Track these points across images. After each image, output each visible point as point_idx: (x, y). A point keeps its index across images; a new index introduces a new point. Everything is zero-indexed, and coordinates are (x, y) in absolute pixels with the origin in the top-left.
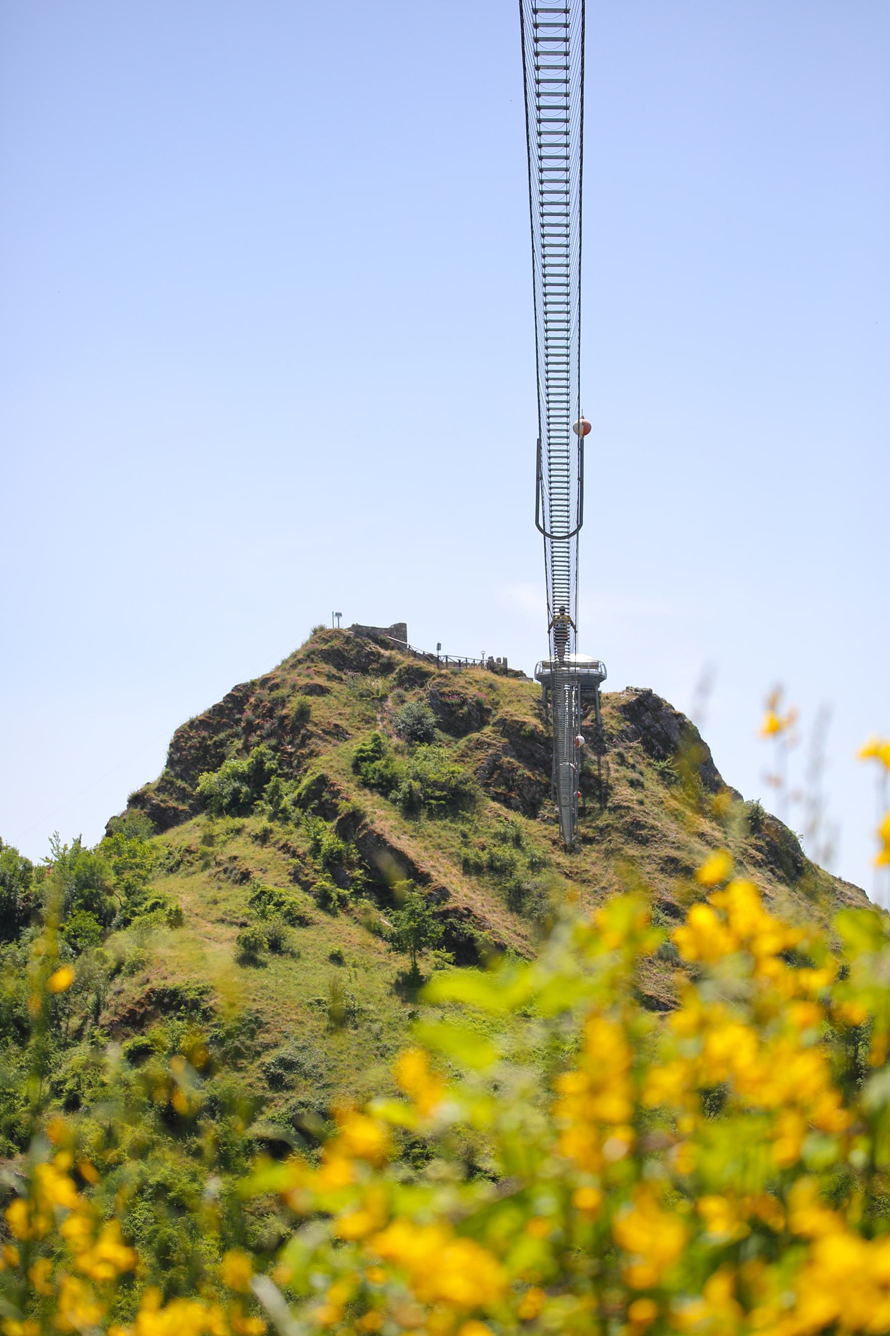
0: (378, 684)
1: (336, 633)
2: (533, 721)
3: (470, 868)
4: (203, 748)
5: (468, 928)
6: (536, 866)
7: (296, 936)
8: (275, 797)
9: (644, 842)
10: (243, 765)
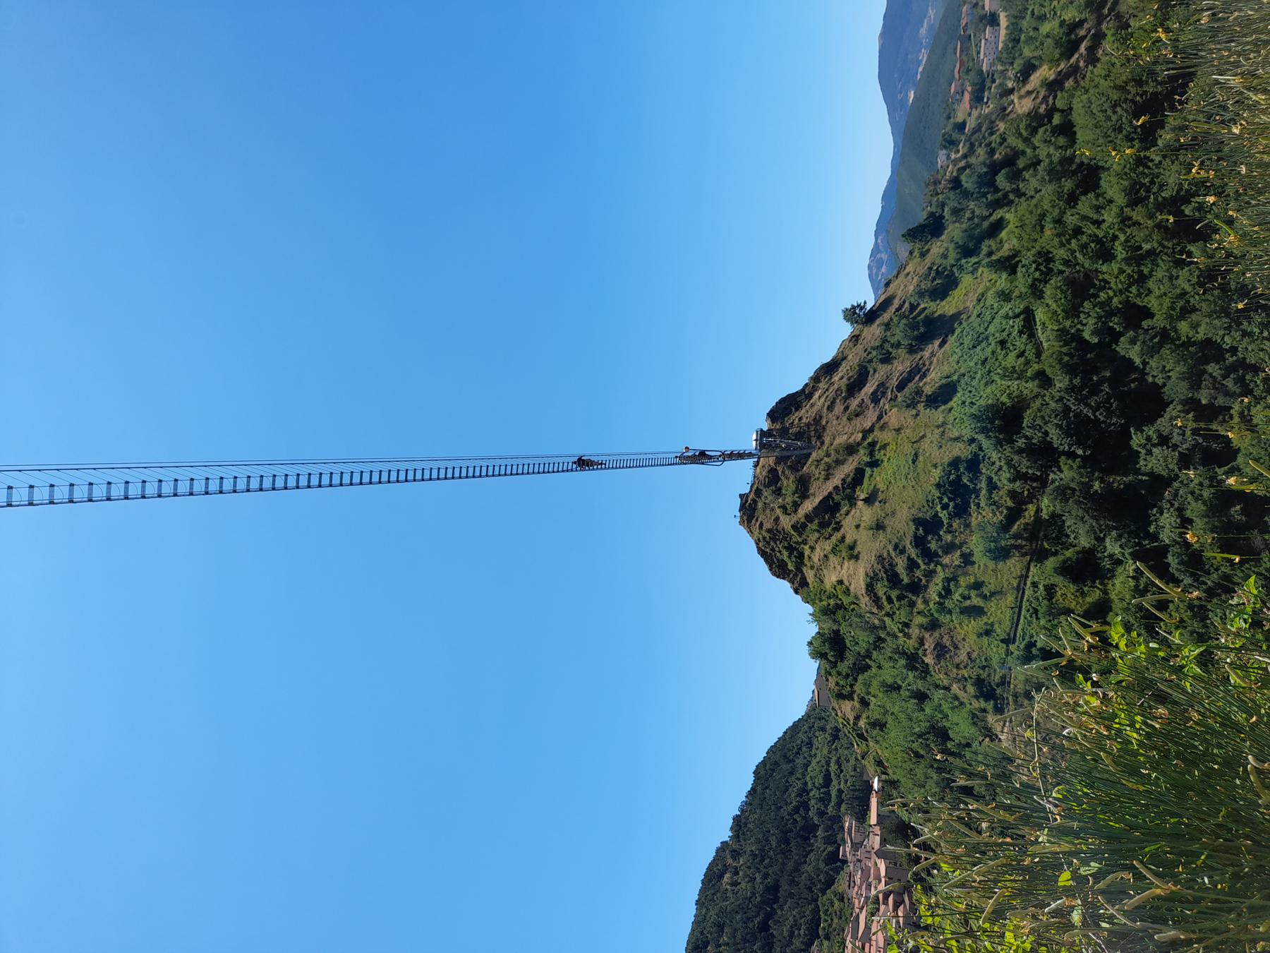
0: (760, 505)
3: (827, 478)
5: (849, 480)
7: (848, 540)
8: (797, 543)
9: (821, 417)
10: (786, 553)
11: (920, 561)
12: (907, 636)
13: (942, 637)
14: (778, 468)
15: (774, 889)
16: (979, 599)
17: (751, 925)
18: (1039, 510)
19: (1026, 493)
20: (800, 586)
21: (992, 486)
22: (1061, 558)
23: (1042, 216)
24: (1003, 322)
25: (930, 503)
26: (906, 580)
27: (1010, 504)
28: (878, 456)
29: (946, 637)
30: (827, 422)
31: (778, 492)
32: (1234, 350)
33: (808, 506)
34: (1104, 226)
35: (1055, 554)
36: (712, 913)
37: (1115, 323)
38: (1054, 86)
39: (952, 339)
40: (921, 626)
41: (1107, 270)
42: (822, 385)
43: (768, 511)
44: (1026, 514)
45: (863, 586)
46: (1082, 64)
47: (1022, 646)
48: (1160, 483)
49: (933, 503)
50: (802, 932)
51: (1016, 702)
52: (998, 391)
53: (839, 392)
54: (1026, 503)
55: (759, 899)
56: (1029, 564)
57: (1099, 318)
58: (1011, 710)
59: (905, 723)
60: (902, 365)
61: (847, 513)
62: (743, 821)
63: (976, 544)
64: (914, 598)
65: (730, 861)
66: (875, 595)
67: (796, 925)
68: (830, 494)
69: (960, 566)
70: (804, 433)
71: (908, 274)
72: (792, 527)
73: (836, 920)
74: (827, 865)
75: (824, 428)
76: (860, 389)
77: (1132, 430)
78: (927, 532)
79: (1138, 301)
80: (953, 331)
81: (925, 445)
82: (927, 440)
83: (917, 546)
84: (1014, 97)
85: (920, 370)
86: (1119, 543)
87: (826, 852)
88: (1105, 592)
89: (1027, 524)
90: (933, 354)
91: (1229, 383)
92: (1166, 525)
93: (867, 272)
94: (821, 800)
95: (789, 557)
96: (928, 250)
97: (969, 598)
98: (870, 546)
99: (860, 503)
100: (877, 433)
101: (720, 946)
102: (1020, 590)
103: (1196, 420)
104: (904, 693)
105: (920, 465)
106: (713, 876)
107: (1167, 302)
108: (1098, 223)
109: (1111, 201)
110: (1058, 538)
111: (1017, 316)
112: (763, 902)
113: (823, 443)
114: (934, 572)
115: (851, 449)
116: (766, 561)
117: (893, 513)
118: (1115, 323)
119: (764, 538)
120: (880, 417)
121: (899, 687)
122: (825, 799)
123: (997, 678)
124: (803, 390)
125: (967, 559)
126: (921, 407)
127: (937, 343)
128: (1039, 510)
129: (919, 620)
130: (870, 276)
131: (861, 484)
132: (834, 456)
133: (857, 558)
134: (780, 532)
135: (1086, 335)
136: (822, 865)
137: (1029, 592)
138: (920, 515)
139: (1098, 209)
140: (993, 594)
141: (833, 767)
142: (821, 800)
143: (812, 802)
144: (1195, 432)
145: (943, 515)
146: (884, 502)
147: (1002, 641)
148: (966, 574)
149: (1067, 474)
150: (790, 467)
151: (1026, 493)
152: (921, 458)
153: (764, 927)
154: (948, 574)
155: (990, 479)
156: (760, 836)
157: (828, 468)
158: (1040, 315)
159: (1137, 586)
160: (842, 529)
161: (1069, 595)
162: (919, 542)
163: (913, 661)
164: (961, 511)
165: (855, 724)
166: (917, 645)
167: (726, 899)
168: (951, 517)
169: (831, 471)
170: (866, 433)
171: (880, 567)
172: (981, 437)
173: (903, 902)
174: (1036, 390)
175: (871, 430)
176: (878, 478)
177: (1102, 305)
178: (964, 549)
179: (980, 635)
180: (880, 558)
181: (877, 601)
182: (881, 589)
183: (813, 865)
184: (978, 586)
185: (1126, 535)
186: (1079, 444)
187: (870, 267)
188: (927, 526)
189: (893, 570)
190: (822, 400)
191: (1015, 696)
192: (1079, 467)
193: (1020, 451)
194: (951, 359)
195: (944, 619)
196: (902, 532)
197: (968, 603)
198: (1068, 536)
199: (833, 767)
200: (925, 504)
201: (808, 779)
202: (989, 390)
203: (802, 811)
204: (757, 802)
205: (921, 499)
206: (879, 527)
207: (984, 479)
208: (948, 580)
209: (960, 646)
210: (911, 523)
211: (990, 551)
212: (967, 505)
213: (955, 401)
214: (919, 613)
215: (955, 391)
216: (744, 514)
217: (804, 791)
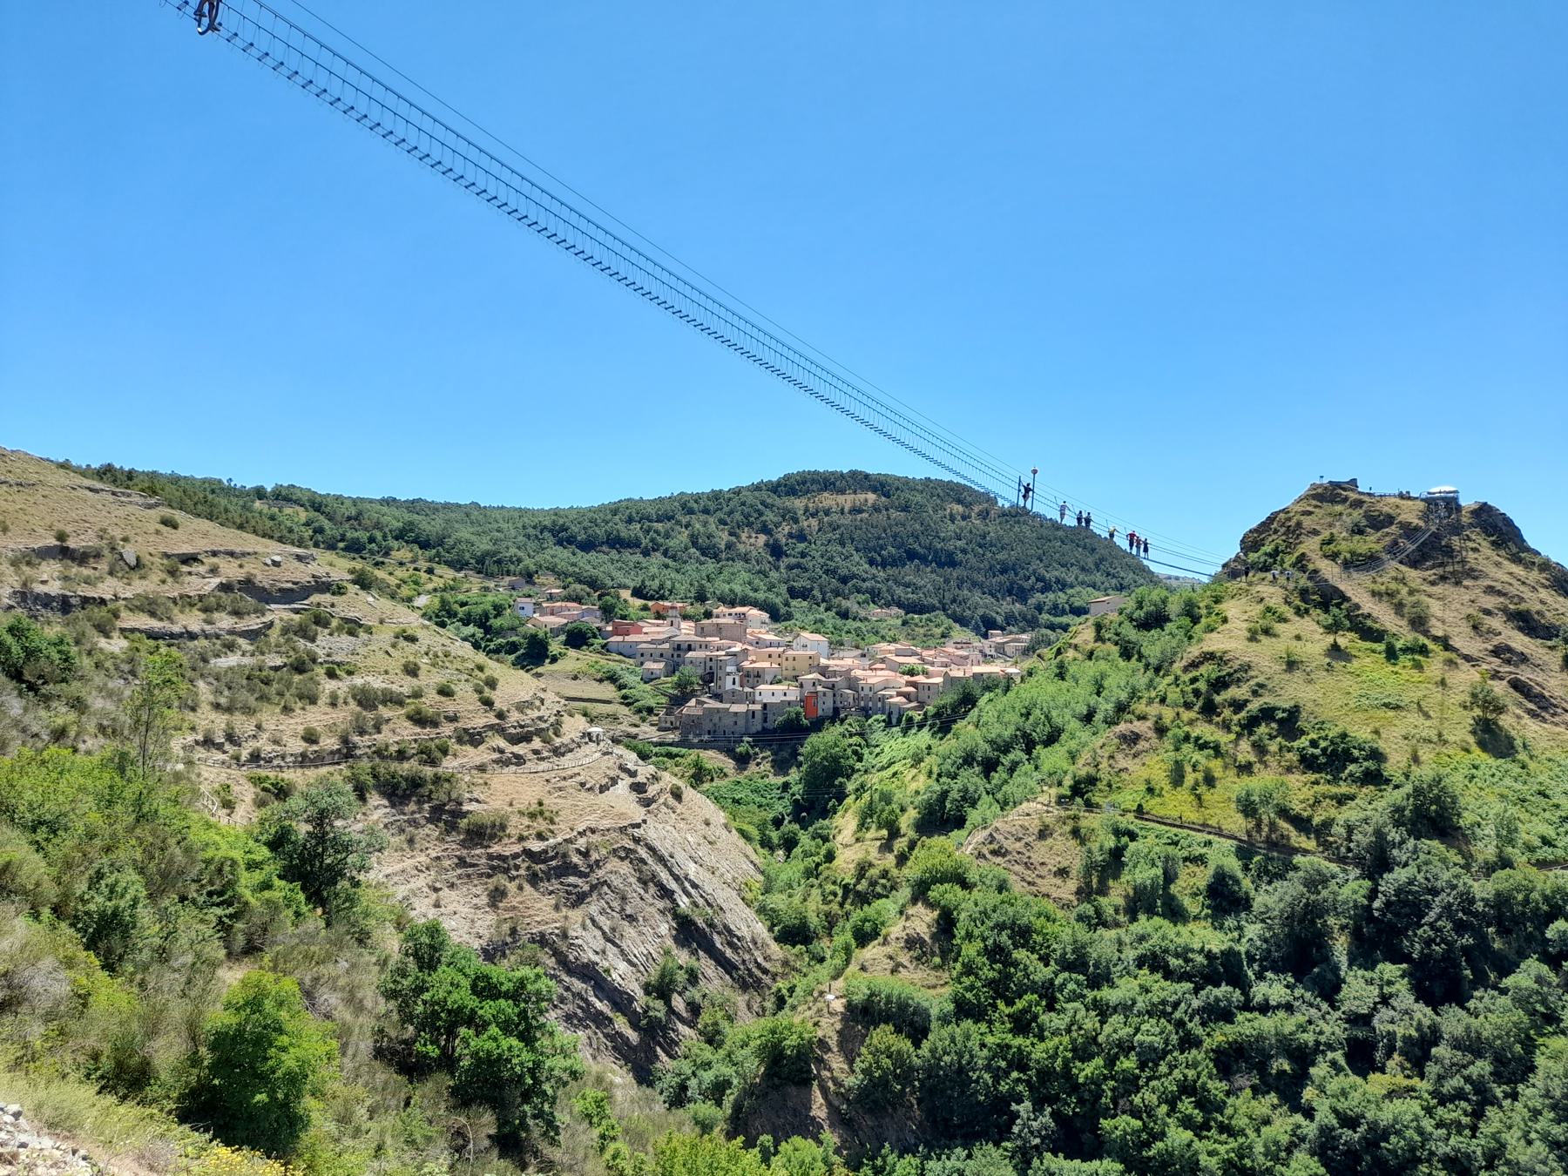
0: (1339, 508)
1: (1321, 486)
3: (1374, 594)
5: (1369, 623)
7: (1279, 628)
8: (1283, 562)
9: (1475, 578)
11: (1243, 714)
13: (1147, 740)
14: (1393, 527)
15: (953, 564)
16: (1192, 782)
17: (911, 540)
18: (1305, 852)
19: (1331, 839)
20: (1232, 571)
22: (1240, 875)
26: (1218, 699)
27: (1316, 820)
29: (1147, 745)
30: (1467, 588)
31: (1358, 530)
33: (1330, 572)
35: (1246, 868)
36: (919, 498)
42: (1534, 576)
43: (1329, 519)
44: (1303, 838)
45: (1211, 649)
47: (1131, 827)
48: (1329, 990)
49: (1321, 729)
50: (910, 596)
53: (1516, 600)
54: (1317, 838)
55: (939, 546)
56: (1235, 838)
58: (1057, 812)
59: (1061, 701)
62: (1022, 519)
63: (1262, 781)
64: (1196, 708)
65: (976, 509)
66: (1202, 663)
67: (916, 589)
68: (1348, 599)
69: (1235, 760)
70: (1452, 557)
72: (1303, 554)
73: (922, 631)
74: (982, 617)
75: (1458, 583)
76: (1520, 629)
77: (1405, 966)
81: (1414, 718)
82: (1421, 720)
83: (1261, 710)
85: (1545, 709)
86: (1255, 938)
87: (994, 615)
88: (1196, 918)
89: (1288, 838)
91: (1456, 1082)
92: (1273, 989)
94: (1055, 606)
95: (1266, 554)
97: (1194, 771)
98: (1264, 657)
99: (1330, 639)
101: (887, 510)
103: (1407, 1039)
104: (1093, 700)
105: (1381, 713)
106: (957, 493)
110: (1267, 872)
112: (936, 552)
113: (1433, 583)
114: (1229, 730)
115: (1419, 623)
116: (1263, 524)
119: (1289, 519)
120: (1467, 658)
121: (1098, 694)
122: (1056, 610)
123: (1096, 799)
124: (1528, 550)
125: (1246, 769)
126: (1477, 712)
128: (1305, 852)
131: (1363, 638)
132: (1409, 600)
134: (1297, 538)
136: (981, 612)
137: (1202, 837)
138: (1304, 714)
140: (1199, 797)
142: (1055, 606)
143: (1051, 596)
144: (1391, 1036)
145: (1303, 742)
147: (1140, 806)
148: (1226, 767)
149: (1351, 888)
151: (1331, 839)
152: (1391, 713)
153: (912, 555)
156: (1006, 540)
159: (1192, 951)
160: (1298, 619)
161: (1194, 880)
162: (1267, 714)
164: (1308, 763)
165: (1070, 645)
166: (1137, 712)
167: (935, 511)
169: (1385, 598)
171: (1236, 667)
172: (1408, 788)
173: (910, 701)
174: (1480, 858)
175: (1447, 647)
176: (1368, 660)
178: (1258, 765)
179: (1148, 782)
180: (1247, 668)
181: (1194, 665)
182: (1206, 670)
183: (980, 602)
184: (1210, 781)
185: (1265, 946)
186: (1388, 904)
188: (1289, 724)
189: (1232, 682)
190: (1506, 578)
191: (1075, 818)
192: (1355, 901)
193: (1379, 834)
194: (1558, 751)
195: (1168, 743)
196: (1282, 692)
197: (1188, 769)
198: (1270, 883)
200: (1320, 719)
201: (1078, 589)
203: (1040, 585)
204: (1045, 532)
207: (1353, 790)
209: (1137, 760)
210: (1292, 703)
211: (1248, 795)
214: (1178, 714)
215: (1499, 755)
216: (1326, 488)
217: (1063, 586)
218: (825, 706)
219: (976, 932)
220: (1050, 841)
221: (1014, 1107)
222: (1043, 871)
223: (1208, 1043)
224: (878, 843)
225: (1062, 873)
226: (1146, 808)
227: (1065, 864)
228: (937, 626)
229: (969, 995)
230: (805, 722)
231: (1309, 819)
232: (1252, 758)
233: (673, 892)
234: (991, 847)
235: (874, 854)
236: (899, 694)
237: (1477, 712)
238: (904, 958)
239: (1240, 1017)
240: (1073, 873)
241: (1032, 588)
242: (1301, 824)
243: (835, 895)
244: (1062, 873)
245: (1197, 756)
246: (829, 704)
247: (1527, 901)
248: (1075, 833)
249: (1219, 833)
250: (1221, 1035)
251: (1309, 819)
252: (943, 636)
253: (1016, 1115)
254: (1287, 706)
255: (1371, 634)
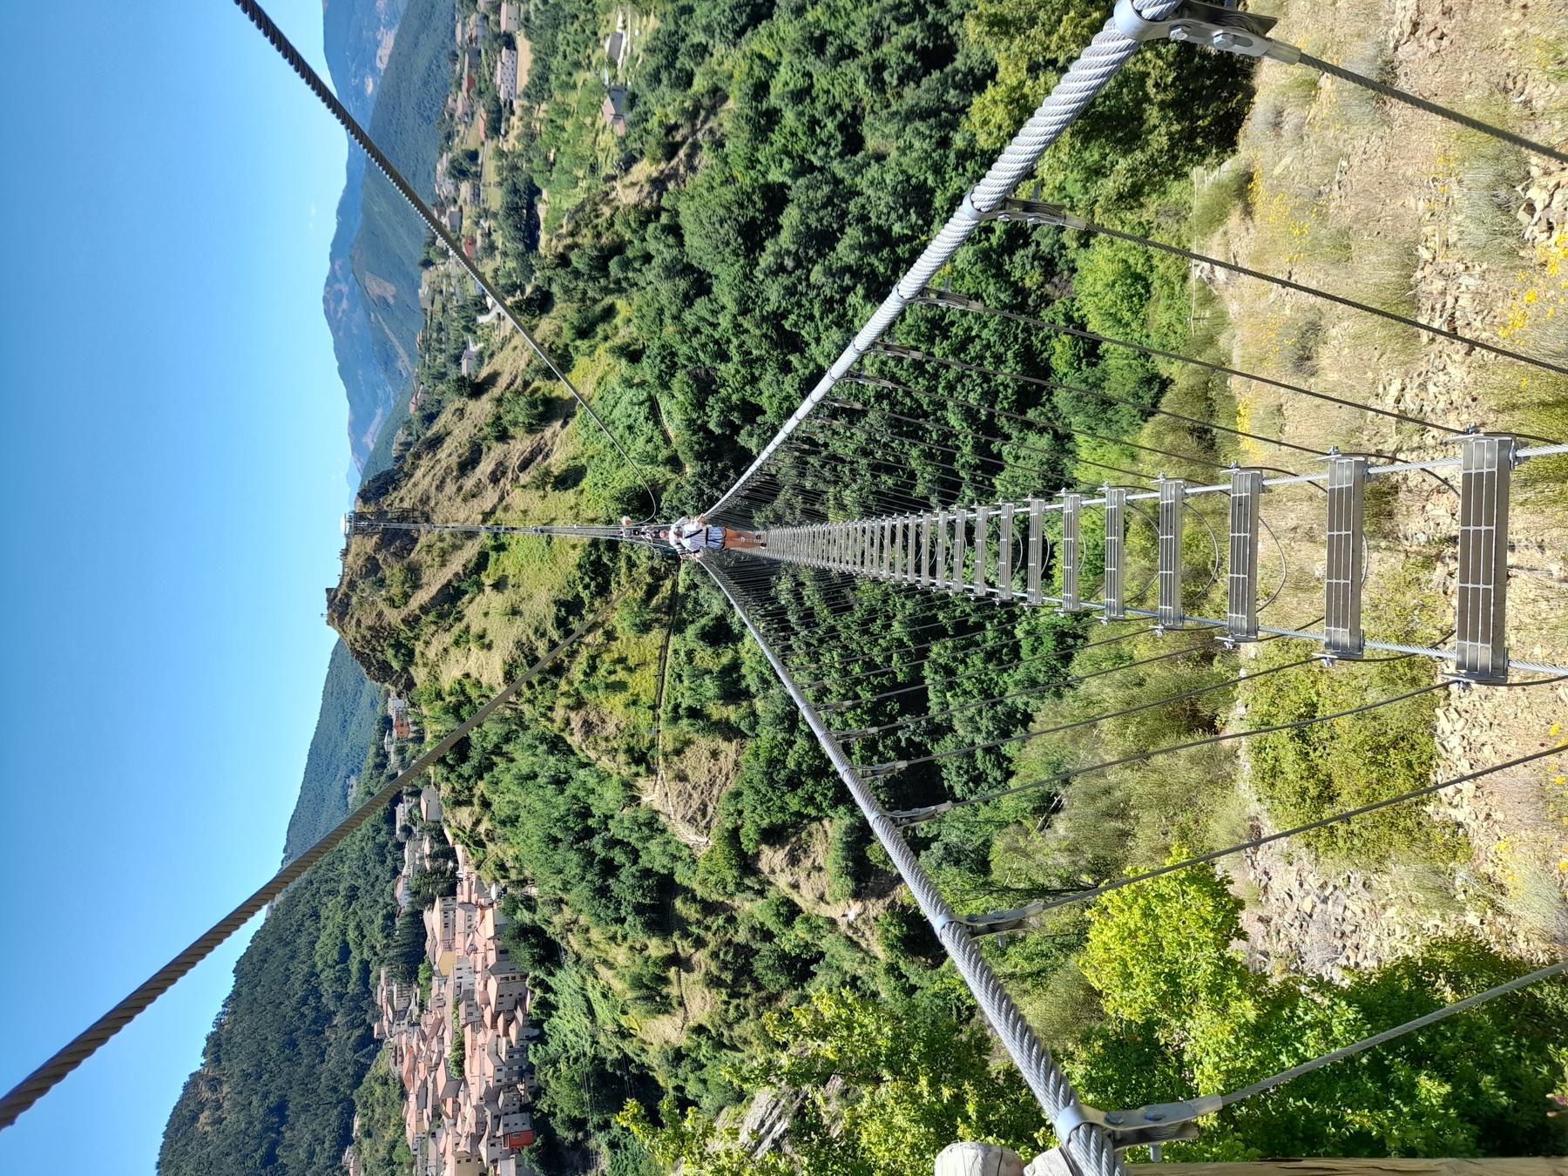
0: (354, 600)
1: (330, 616)
2: (375, 538)
3: (443, 565)
4: (379, 669)
5: (471, 565)
6: (441, 540)
7: (475, 630)
8: (408, 639)
9: (428, 498)
10: (390, 652)
12: (552, 720)
15: (280, 1109)
21: (631, 565)
23: (661, 311)
24: (627, 406)
25: (571, 584)
27: (649, 579)
28: (504, 539)
32: (826, 445)
33: (422, 597)
34: (720, 329)
35: (693, 622)
37: (735, 417)
38: (659, 184)
39: (573, 423)
40: (568, 707)
41: (725, 370)
45: (501, 675)
46: (682, 170)
50: (327, 1145)
51: (666, 760)
52: (631, 475)
55: (259, 1127)
57: (722, 412)
60: (521, 445)
61: (471, 601)
68: (450, 582)
71: (515, 348)
73: (378, 1110)
78: (569, 613)
79: (752, 400)
80: (573, 414)
84: (618, 185)
88: (737, 652)
90: (555, 435)
91: (827, 473)
93: (322, 306)
96: (536, 326)
97: (615, 672)
98: (506, 636)
99: (488, 589)
100: (499, 513)
102: (662, 659)
104: (541, 780)
107: (776, 402)
108: (715, 326)
109: (723, 308)
111: (642, 403)
112: (266, 1130)
117: (531, 597)
118: (735, 417)
119: (364, 637)
120: (502, 499)
125: (610, 636)
127: (560, 423)
128: (675, 584)
129: (563, 701)
130: (327, 312)
133: (489, 647)
135: (712, 426)
136: (349, 1055)
139: (714, 313)
141: (352, 935)
145: (585, 595)
146: (517, 586)
148: (609, 651)
150: (394, 554)
152: (555, 540)
154: (592, 651)
155: (629, 558)
156: (254, 1048)
157: (444, 554)
158: (664, 403)
162: (561, 623)
163: (556, 745)
164: (603, 590)
168: (593, 597)
170: (487, 516)
173: (514, 1018)
175: (493, 511)
177: (725, 400)
180: (519, 644)
184: (622, 660)
187: (325, 300)
188: (570, 608)
190: (428, 479)
191: (666, 755)
197: (613, 678)
199: (352, 935)
202: (621, 473)
203: (312, 1001)
205: (560, 580)
206: (515, 612)
208: (593, 658)
212: (608, 583)
213: (585, 483)
218: (520, 1123)
219: (778, 803)
220: (689, 772)
221: (903, 744)
222: (715, 770)
223: (831, 621)
224: (684, 974)
225: (715, 754)
226: (650, 703)
227: (707, 754)
228: (372, 1094)
229: (830, 794)
230: (539, 1141)
231: (649, 585)
232: (601, 631)
233: (774, 1141)
234: (699, 818)
235: (697, 975)
236: (506, 1033)
237: (548, 488)
238: (807, 863)
239: (808, 604)
240: (713, 746)
241: (317, 1009)
242: (652, 591)
243: (738, 1007)
244: (715, 754)
245: (602, 672)
246: (517, 1118)
247: (700, 444)
248: (678, 752)
249: (664, 648)
250: (823, 612)
251: (649, 585)
252: (385, 1083)
253: (909, 740)
254: (555, 609)
255: (482, 562)
